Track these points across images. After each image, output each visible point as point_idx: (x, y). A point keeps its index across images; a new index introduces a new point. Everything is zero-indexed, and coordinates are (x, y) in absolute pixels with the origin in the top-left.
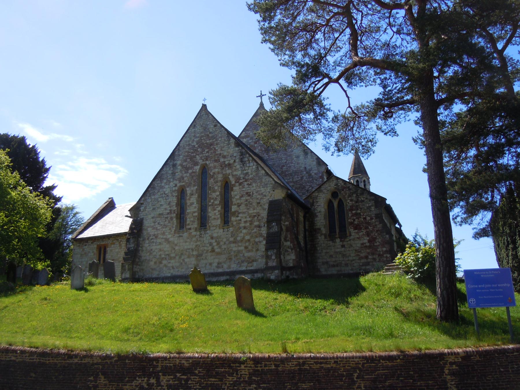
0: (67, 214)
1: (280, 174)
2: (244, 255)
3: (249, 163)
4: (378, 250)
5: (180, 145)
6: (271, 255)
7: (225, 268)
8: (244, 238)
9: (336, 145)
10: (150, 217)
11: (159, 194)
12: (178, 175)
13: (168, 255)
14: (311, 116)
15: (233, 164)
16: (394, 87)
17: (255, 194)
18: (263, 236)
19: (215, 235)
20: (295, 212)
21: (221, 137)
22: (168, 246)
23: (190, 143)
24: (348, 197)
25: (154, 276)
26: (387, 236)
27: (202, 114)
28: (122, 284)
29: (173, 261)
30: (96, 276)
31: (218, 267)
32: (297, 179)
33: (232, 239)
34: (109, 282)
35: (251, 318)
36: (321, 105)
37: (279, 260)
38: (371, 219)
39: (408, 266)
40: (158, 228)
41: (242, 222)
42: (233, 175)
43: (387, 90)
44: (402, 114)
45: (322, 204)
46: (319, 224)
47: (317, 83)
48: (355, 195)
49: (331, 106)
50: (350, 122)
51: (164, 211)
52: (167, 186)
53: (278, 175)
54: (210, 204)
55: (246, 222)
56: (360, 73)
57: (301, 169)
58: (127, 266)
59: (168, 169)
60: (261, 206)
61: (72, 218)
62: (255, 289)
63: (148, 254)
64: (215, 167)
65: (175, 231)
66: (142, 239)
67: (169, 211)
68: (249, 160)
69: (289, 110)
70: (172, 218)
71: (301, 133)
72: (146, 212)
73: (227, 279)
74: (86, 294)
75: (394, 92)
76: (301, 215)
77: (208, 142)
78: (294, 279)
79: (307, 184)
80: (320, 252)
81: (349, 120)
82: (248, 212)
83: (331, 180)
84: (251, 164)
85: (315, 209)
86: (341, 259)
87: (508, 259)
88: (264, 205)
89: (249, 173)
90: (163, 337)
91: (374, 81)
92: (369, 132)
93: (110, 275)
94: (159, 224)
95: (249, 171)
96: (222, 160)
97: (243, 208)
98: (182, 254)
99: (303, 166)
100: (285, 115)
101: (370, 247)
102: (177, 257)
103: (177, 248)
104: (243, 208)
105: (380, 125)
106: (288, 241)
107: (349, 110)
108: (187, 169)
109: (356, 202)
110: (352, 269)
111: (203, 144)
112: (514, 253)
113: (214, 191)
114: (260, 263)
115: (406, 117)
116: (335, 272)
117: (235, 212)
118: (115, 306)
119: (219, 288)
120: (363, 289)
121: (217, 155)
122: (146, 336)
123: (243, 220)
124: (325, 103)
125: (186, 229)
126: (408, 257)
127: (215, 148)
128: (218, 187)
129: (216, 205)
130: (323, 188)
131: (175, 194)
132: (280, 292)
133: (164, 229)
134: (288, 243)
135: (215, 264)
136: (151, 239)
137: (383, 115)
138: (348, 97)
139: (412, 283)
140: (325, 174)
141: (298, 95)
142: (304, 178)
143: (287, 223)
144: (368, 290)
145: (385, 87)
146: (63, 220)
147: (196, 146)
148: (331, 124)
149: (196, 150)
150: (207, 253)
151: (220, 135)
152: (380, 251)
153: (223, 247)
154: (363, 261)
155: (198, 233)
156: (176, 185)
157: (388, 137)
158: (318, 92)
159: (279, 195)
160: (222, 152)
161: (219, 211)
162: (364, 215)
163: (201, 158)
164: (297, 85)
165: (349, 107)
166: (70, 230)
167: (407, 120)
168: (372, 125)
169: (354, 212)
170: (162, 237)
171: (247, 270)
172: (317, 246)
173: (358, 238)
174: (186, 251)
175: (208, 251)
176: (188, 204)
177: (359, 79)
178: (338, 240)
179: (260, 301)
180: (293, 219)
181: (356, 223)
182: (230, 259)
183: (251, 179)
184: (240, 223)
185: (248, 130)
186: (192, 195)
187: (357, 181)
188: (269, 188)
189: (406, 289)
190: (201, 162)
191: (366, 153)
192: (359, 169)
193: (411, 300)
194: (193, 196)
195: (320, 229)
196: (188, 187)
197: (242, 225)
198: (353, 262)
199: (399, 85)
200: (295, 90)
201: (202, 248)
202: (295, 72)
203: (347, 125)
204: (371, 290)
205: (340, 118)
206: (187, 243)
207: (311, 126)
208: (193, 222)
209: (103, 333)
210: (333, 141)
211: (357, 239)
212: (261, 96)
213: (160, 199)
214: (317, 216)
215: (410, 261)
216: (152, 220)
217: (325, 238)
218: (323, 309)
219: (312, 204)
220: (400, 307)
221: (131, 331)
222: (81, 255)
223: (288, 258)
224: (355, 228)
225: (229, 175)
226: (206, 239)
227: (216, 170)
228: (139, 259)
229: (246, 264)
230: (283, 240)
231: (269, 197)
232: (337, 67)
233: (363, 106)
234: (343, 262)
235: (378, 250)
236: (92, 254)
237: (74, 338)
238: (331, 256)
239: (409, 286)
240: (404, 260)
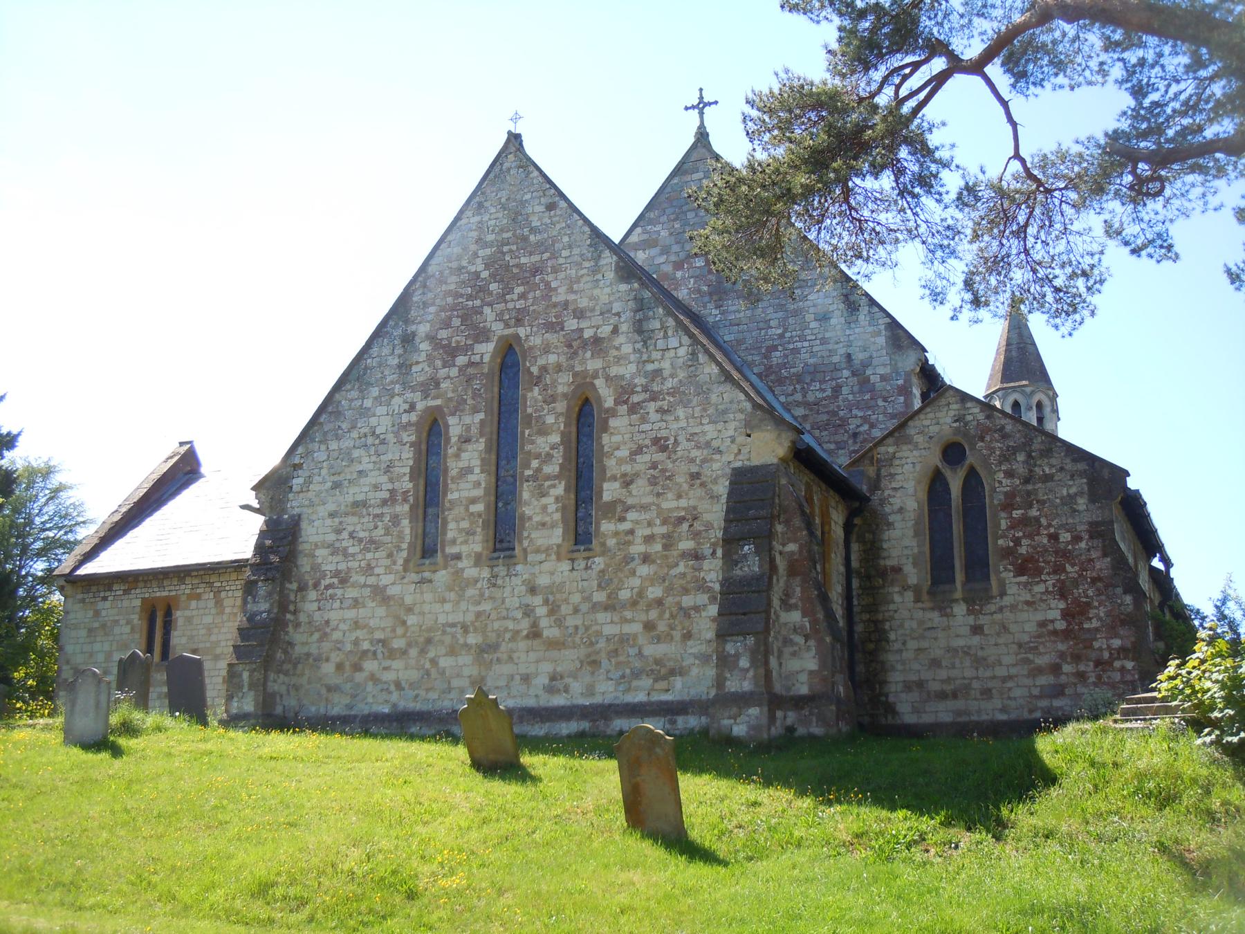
0: (27, 489)
1: (759, 375)
2: (640, 653)
3: (666, 337)
4: (1096, 645)
5: (431, 269)
6: (737, 656)
7: (576, 694)
8: (641, 594)
9: (968, 284)
10: (322, 511)
11: (355, 434)
12: (420, 372)
13: (383, 642)
14: (886, 181)
15: (610, 339)
16: (1171, 93)
17: (684, 444)
18: (710, 589)
19: (543, 581)
20: (817, 511)
21: (570, 247)
22: (381, 611)
23: (464, 263)
24: (1000, 463)
25: (335, 711)
26: (1128, 599)
27: (506, 165)
28: (232, 734)
29: (397, 664)
30: (142, 703)
31: (550, 690)
32: (820, 395)
33: (600, 597)
34: (185, 725)
35: (677, 866)
36: (924, 151)
37: (762, 671)
38: (1077, 539)
39: (1201, 703)
40: (351, 550)
41: (639, 540)
42: (608, 378)
43: (1146, 102)
44: (1193, 185)
45: (910, 486)
46: (895, 553)
47: (907, 71)
48: (1021, 457)
49: (956, 152)
50: (1016, 205)
51: (371, 495)
52: (381, 410)
53: (754, 378)
54: (528, 473)
55: (649, 539)
56: (1054, 42)
57: (836, 359)
58: (246, 675)
59: (386, 351)
60: (703, 485)
61: (46, 503)
62: (685, 769)
63: (316, 636)
64: (546, 350)
65: (407, 561)
66: (294, 586)
67: (386, 495)
68: (664, 328)
69: (817, 161)
70: (395, 520)
71: (846, 238)
72: (310, 495)
73: (589, 733)
74: (118, 763)
75: (1169, 111)
76: (837, 518)
77: (523, 260)
78: (812, 738)
79: (855, 412)
80: (896, 646)
81: (1013, 200)
82: (658, 506)
83: (943, 401)
84: (673, 342)
85: (883, 502)
86: (969, 673)
88: (715, 481)
89: (666, 373)
90: (384, 917)
91: (1102, 71)
92: (1080, 245)
93: (189, 701)
94: (351, 536)
95: (666, 365)
96: (571, 324)
97: (641, 492)
98: (429, 641)
99: (842, 351)
100: (802, 179)
101: (1066, 634)
102: (413, 652)
103: (412, 620)
104: (641, 492)
105: (1117, 219)
106: (795, 607)
107: (1016, 166)
108: (451, 352)
109: (1027, 481)
110: (1004, 710)
111: (507, 267)
113: (543, 432)
114: (697, 681)
115: (1209, 197)
116: (946, 718)
117: (612, 505)
118: (216, 807)
119: (561, 760)
120: (1050, 779)
121: (555, 305)
122: (329, 910)
123: (642, 532)
124: (933, 140)
125: (445, 556)
126: (1203, 674)
127: (548, 284)
128: (558, 415)
129: (548, 478)
130: (911, 430)
131: (409, 437)
132: (767, 783)
133: (369, 556)
134: (795, 617)
135: (543, 680)
136: (327, 587)
137: (1131, 188)
138: (1014, 125)
139: (1214, 761)
140: (915, 380)
141: (845, 111)
142: (845, 390)
143: (792, 547)
144: (1065, 782)
145: (1139, 92)
146: (16, 511)
147: (485, 274)
148: (952, 211)
149: (483, 290)
150: (513, 639)
151: (566, 239)
152: (1100, 649)
153: (571, 622)
154: (1043, 680)
155: (486, 573)
156: (412, 407)
157: (1144, 262)
158: (912, 103)
159: (768, 448)
160: (572, 297)
161: (557, 499)
162: (1050, 525)
163: (499, 317)
164: (843, 76)
165: (1017, 156)
166: (39, 545)
167: (1210, 206)
168: (1092, 221)
169: (1017, 514)
170: (362, 580)
171: (650, 704)
172: (887, 626)
173: (1028, 603)
174: (444, 632)
175: (517, 633)
176: (453, 473)
177: (1051, 63)
178: (960, 609)
179: (702, 810)
180: (811, 534)
181: (1023, 550)
182: (595, 664)
183: (673, 392)
184: (629, 543)
185: (652, 222)
186: (467, 441)
187: (1016, 405)
188: (732, 425)
189: (1194, 781)
190: (498, 329)
191: (1068, 314)
192: (1021, 361)
193: (1211, 816)
194: (470, 447)
195: (898, 570)
196: (453, 414)
197: (638, 548)
198: (1010, 684)
199: (1188, 87)
200: (834, 96)
201: (496, 625)
202: (836, 34)
203: (1008, 218)
204: (1076, 778)
205: (986, 194)
206: (448, 607)
207: (882, 217)
208: (470, 533)
209: (186, 895)
210: (957, 270)
211: (1025, 609)
212: (701, 106)
213: (356, 453)
214: (890, 525)
215: (1211, 687)
216: (329, 522)
217: (918, 600)
218: (916, 842)
219: (876, 485)
220: (1177, 842)
221: (279, 892)
222: (90, 631)
223: (793, 665)
224: (1021, 571)
225: (595, 375)
226: (513, 591)
227: (552, 359)
228: (285, 652)
229: (646, 682)
230: (776, 602)
231: (731, 458)
232: (976, 20)
233: (1063, 156)
234: (976, 684)
235: (1096, 645)
236: (127, 629)
237: (92, 908)
238: (935, 663)
239: (1204, 772)
240: (1187, 683)
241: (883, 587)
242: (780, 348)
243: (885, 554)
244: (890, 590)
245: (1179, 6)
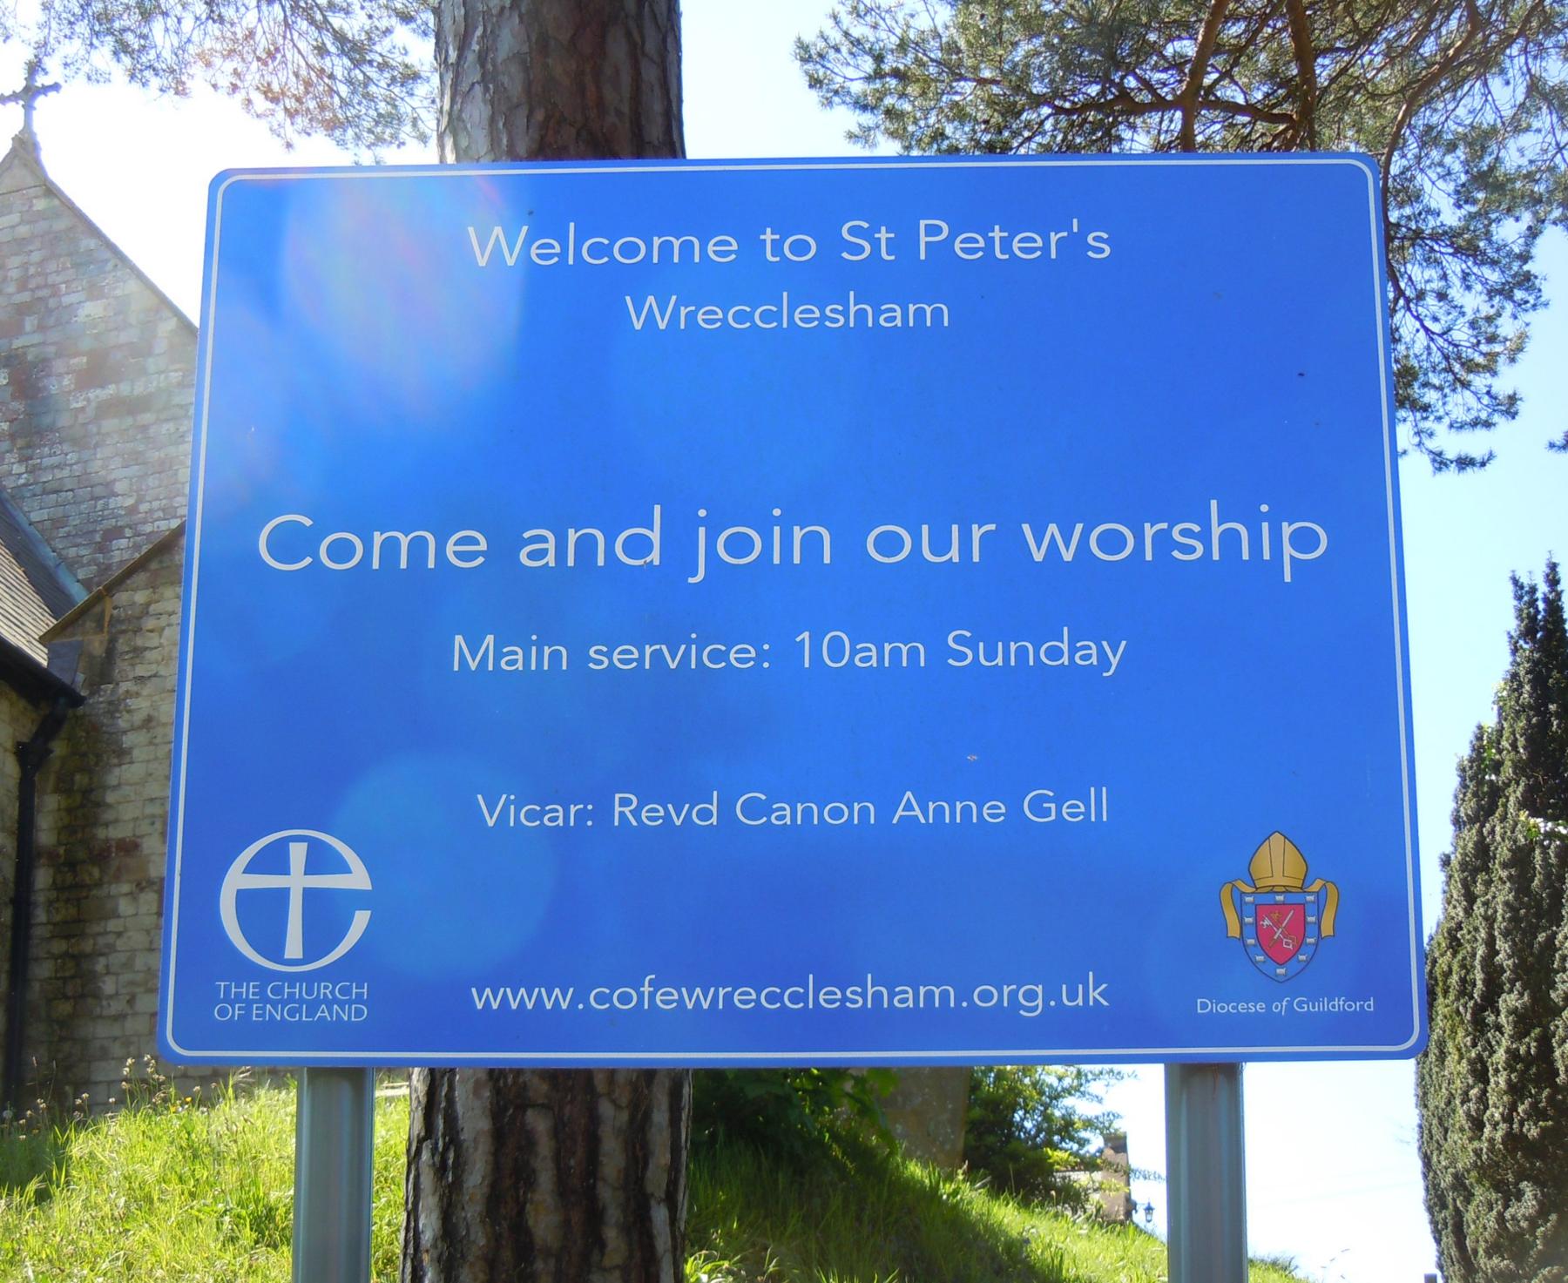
46: (128, 812)
80: (116, 1007)
85: (114, 707)
87: (1483, 1098)
112: (1529, 1045)
214: (122, 754)
219: (103, 672)
241: (99, 884)
242: (128, 532)
243: (108, 816)
244: (114, 889)
245: (847, 1270)
